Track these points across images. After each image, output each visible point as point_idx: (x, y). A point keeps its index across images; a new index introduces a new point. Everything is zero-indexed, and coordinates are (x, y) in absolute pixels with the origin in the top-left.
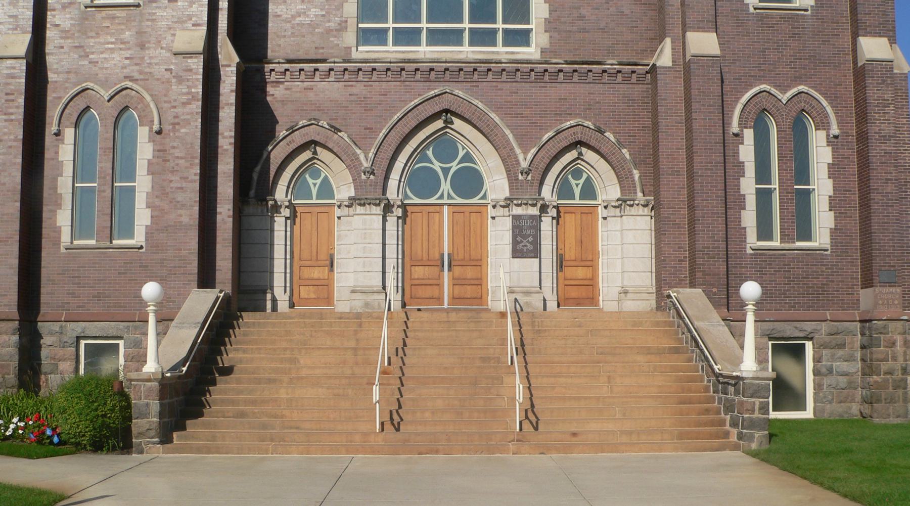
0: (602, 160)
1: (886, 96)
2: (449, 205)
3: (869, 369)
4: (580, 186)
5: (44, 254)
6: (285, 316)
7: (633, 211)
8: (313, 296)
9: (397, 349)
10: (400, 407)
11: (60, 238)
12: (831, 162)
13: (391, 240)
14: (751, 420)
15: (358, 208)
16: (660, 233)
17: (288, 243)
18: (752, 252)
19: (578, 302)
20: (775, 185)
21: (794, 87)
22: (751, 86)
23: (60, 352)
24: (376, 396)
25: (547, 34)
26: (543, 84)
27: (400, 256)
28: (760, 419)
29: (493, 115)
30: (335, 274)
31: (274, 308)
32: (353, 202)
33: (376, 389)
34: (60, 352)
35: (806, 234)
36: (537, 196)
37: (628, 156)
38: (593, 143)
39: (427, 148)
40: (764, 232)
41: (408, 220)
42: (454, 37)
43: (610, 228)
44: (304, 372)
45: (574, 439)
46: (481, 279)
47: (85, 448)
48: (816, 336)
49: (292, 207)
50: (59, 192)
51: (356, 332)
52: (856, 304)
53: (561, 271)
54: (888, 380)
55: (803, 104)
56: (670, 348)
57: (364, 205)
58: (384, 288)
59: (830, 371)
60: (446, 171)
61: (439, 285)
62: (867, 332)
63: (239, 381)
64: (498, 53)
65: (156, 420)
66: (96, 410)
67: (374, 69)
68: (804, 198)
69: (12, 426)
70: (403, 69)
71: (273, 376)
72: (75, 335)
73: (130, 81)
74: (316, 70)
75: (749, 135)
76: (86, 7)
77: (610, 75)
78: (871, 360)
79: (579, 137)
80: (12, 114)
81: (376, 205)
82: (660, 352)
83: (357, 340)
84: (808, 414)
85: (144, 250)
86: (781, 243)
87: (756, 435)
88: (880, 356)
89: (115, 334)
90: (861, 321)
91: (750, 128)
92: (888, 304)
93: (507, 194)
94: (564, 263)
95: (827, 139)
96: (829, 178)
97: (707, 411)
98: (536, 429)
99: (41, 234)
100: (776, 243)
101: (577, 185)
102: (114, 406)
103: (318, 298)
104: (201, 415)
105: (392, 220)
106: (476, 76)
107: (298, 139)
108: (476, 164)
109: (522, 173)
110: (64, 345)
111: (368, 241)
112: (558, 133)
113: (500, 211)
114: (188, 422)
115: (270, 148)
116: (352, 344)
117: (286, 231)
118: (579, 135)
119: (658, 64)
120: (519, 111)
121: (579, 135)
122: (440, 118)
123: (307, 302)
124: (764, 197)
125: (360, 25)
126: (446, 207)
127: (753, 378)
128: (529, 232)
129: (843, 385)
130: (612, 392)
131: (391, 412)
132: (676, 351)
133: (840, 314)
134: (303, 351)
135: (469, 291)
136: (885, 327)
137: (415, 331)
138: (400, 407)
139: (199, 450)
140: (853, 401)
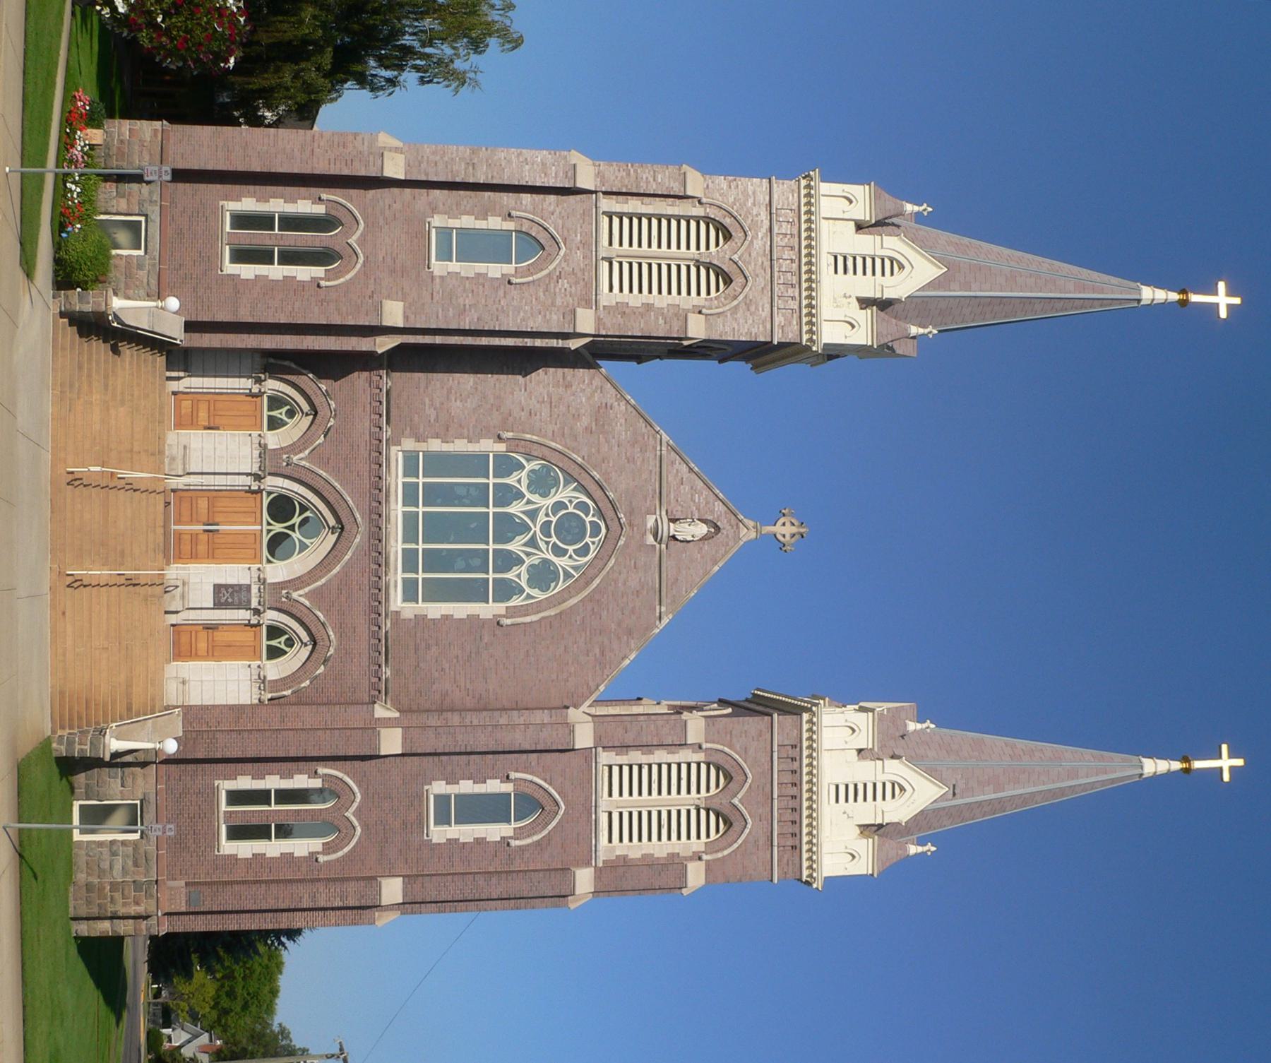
0: (301, 664)
1: (350, 898)
2: (262, 531)
4: (278, 645)
5: (219, 186)
6: (163, 387)
7: (255, 690)
8: (183, 412)
9: (131, 484)
10: (85, 486)
11: (232, 200)
12: (295, 855)
13: (230, 480)
14: (74, 742)
15: (258, 452)
16: (238, 710)
17: (229, 391)
18: (216, 785)
19: (176, 643)
21: (360, 824)
22: (359, 786)
23: (134, 201)
24: (92, 469)
25: (413, 617)
26: (367, 613)
27: (216, 488)
28: (74, 749)
30: (201, 432)
31: (169, 379)
32: (263, 447)
33: (98, 469)
34: (134, 201)
36: (267, 605)
37: (303, 685)
39: (313, 512)
40: (236, 797)
41: (249, 495)
42: (410, 536)
43: (240, 670)
44: (112, 412)
45: (61, 613)
46: (197, 558)
47: (56, 252)
48: (144, 841)
49: (260, 394)
50: (271, 200)
51: (146, 451)
53: (204, 628)
54: (106, 899)
55: (345, 831)
56: (131, 704)
57: (260, 457)
58: (189, 474)
59: (114, 854)
60: (292, 528)
61: (191, 522)
63: (106, 361)
64: (396, 573)
65: (78, 309)
66: (85, 264)
67: (380, 466)
69: (73, 187)
70: (380, 490)
71: (110, 388)
72: (149, 213)
73: (364, 261)
74: (381, 416)
76: (429, 223)
77: (376, 672)
79: (320, 643)
80: (335, 164)
81: (260, 467)
83: (140, 452)
84: (77, 836)
85: (220, 273)
86: (225, 812)
87: (62, 747)
88: (126, 892)
89: (149, 247)
90: (157, 881)
91: (323, 785)
92: (171, 899)
93: (269, 581)
94: (210, 631)
95: (315, 852)
96: (281, 854)
97: (80, 718)
98: (68, 586)
99: (235, 184)
100: (224, 807)
102: (88, 276)
103: (181, 417)
104: (81, 336)
105: (248, 481)
106: (374, 554)
107: (319, 400)
109: (287, 593)
110: (141, 203)
111: (229, 460)
112: (323, 624)
113: (255, 575)
114: (75, 328)
115: (311, 375)
116: (136, 449)
117: (239, 389)
118: (321, 643)
119: (376, 705)
120: (344, 592)
121: (321, 643)
122: (337, 523)
123: (178, 407)
125: (421, 454)
126: (260, 527)
127: (104, 743)
128: (236, 598)
130: (95, 649)
131: (81, 479)
133: (163, 863)
134: (131, 410)
135: (186, 548)
136: (151, 896)
137: (148, 499)
138: (85, 486)
139: (55, 340)
140: (88, 874)
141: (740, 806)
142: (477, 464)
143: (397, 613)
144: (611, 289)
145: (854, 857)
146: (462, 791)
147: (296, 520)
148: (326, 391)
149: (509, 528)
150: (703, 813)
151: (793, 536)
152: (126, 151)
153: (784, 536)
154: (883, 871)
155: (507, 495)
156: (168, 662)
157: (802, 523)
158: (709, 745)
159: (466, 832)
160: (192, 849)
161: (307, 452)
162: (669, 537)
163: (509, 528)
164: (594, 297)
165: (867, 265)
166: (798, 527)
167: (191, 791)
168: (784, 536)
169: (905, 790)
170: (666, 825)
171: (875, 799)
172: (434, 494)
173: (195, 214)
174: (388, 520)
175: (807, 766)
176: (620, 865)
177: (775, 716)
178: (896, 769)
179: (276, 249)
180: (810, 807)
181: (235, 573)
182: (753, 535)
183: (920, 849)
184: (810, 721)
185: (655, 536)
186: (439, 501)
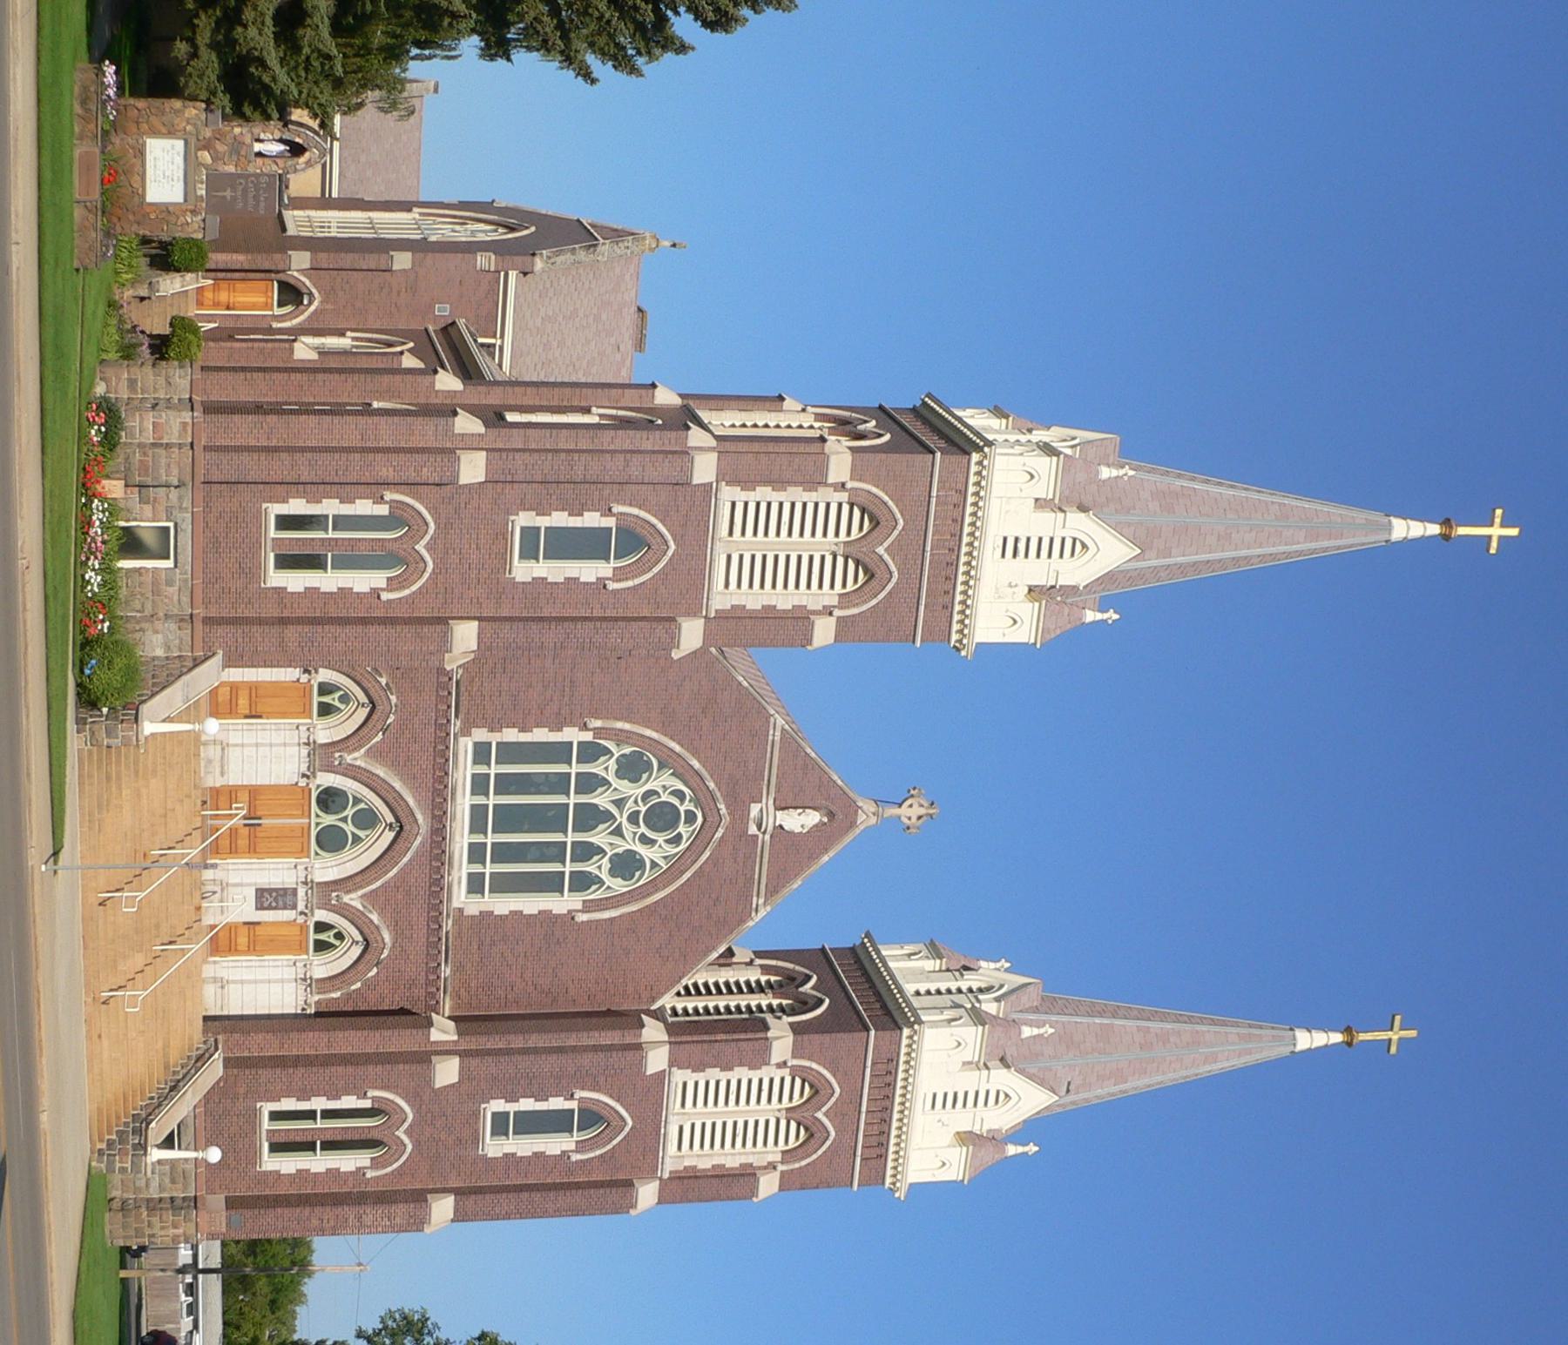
2: (310, 824)
3: (153, 1206)
15: (306, 751)
20: (331, 534)
29: (395, 870)
35: (276, 1148)
37: (353, 987)
38: (367, 957)
39: (367, 804)
40: (285, 522)
46: (236, 852)
52: (211, 1191)
56: (169, 1062)
62: (185, 1204)
68: (309, 1147)
75: (383, 510)
78: (161, 1209)
79: (379, 708)
82: (166, 1055)
88: (164, 1218)
89: (179, 560)
100: (266, 1124)
101: (329, 937)
103: (217, 704)
108: (352, 843)
111: (274, 760)
124: (310, 1115)
126: (307, 821)
129: (137, 1184)
132: (166, 1067)
141: (886, 557)
142: (560, 752)
143: (461, 910)
144: (727, 585)
145: (1032, 476)
146: (522, 1109)
147: (349, 812)
148: (387, 684)
149: (590, 817)
150: (840, 560)
151: (919, 818)
152: (151, 464)
153: (910, 818)
154: (975, 1177)
155: (589, 783)
156: (205, 961)
157: (932, 804)
158: (796, 1062)
159: (523, 1146)
160: (231, 1166)
161: (363, 751)
162: (775, 827)
163: (590, 817)
164: (705, 600)
165: (1044, 548)
166: (927, 808)
167: (232, 1113)
168: (910, 818)
169: (1088, 549)
170: (741, 1133)
171: (1050, 556)
172: (506, 784)
173: (234, 520)
174: (453, 819)
175: (965, 554)
176: (735, 617)
177: (938, 455)
178: (1079, 524)
179: (330, 555)
180: (972, 534)
181: (279, 872)
182: (873, 820)
183: (1099, 616)
184: (980, 463)
185: (759, 827)
186: (513, 788)
